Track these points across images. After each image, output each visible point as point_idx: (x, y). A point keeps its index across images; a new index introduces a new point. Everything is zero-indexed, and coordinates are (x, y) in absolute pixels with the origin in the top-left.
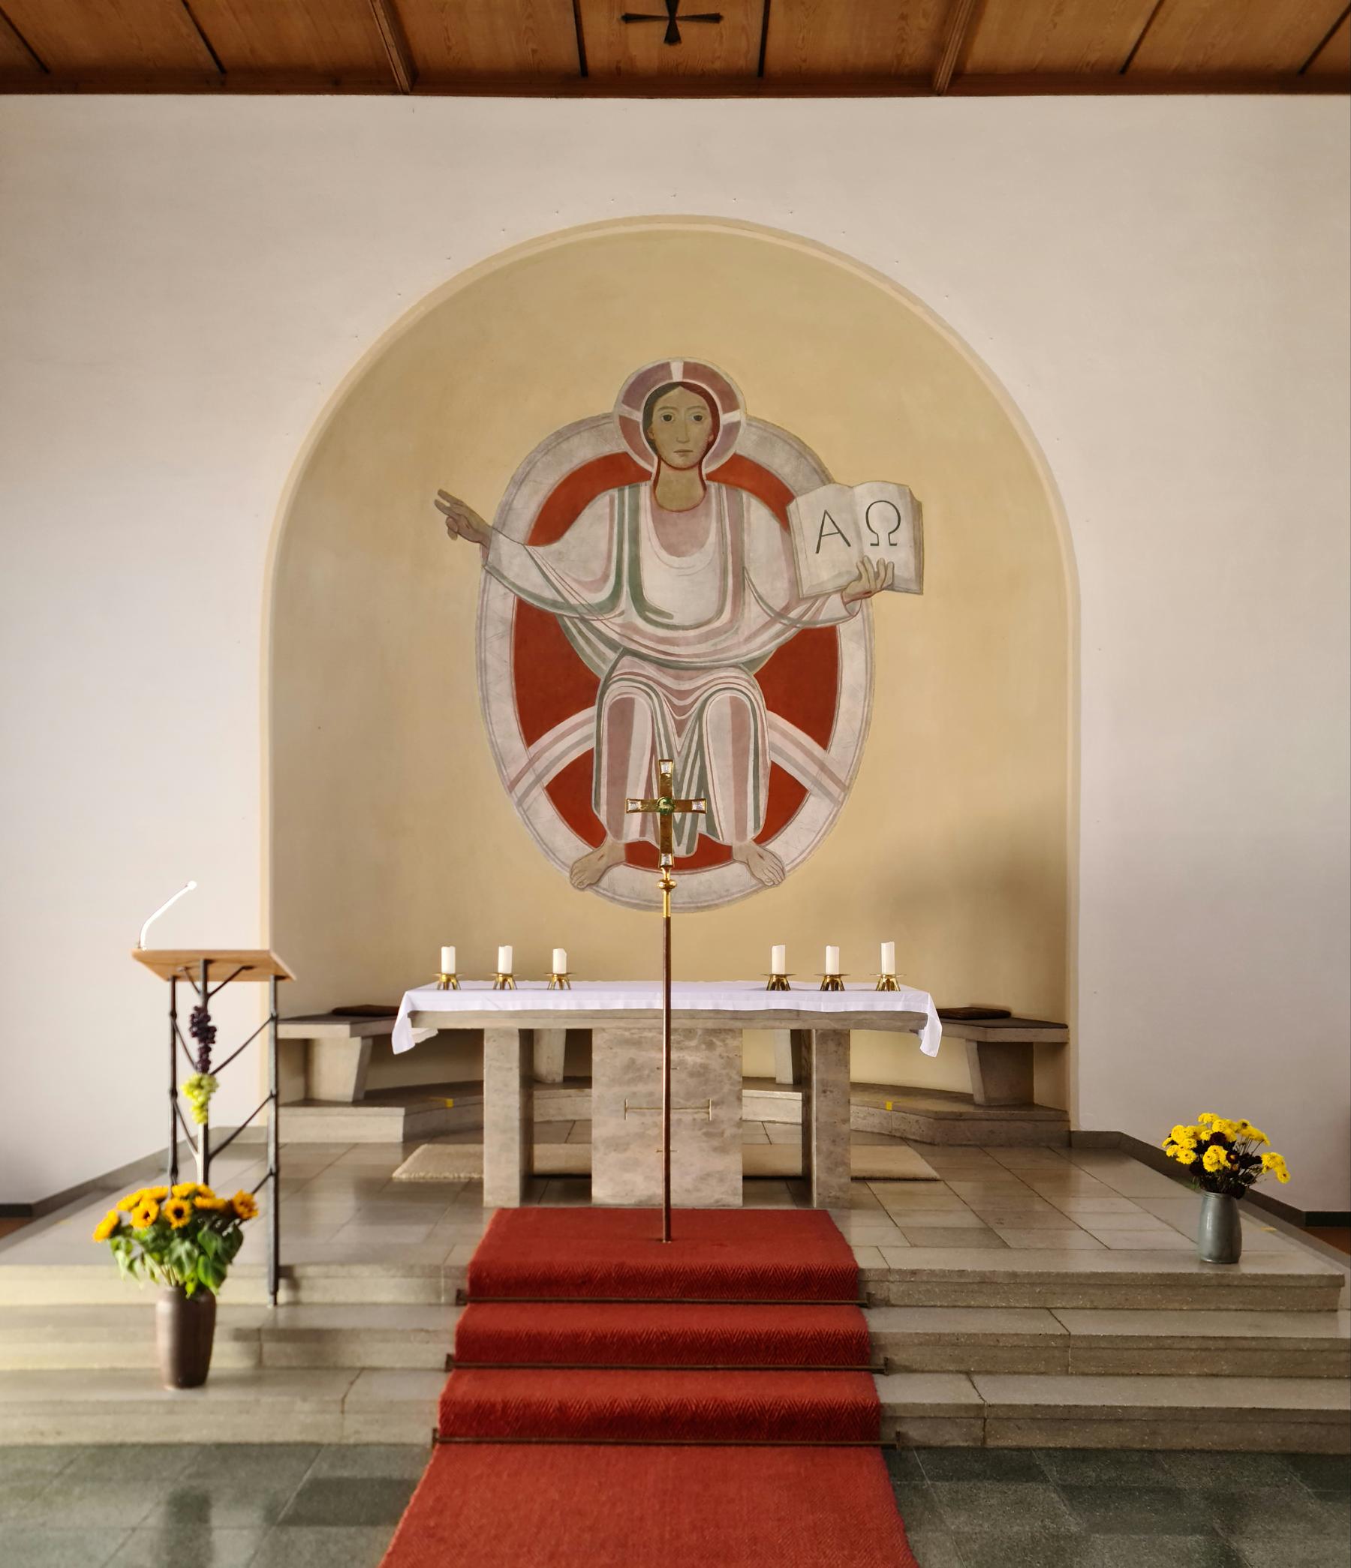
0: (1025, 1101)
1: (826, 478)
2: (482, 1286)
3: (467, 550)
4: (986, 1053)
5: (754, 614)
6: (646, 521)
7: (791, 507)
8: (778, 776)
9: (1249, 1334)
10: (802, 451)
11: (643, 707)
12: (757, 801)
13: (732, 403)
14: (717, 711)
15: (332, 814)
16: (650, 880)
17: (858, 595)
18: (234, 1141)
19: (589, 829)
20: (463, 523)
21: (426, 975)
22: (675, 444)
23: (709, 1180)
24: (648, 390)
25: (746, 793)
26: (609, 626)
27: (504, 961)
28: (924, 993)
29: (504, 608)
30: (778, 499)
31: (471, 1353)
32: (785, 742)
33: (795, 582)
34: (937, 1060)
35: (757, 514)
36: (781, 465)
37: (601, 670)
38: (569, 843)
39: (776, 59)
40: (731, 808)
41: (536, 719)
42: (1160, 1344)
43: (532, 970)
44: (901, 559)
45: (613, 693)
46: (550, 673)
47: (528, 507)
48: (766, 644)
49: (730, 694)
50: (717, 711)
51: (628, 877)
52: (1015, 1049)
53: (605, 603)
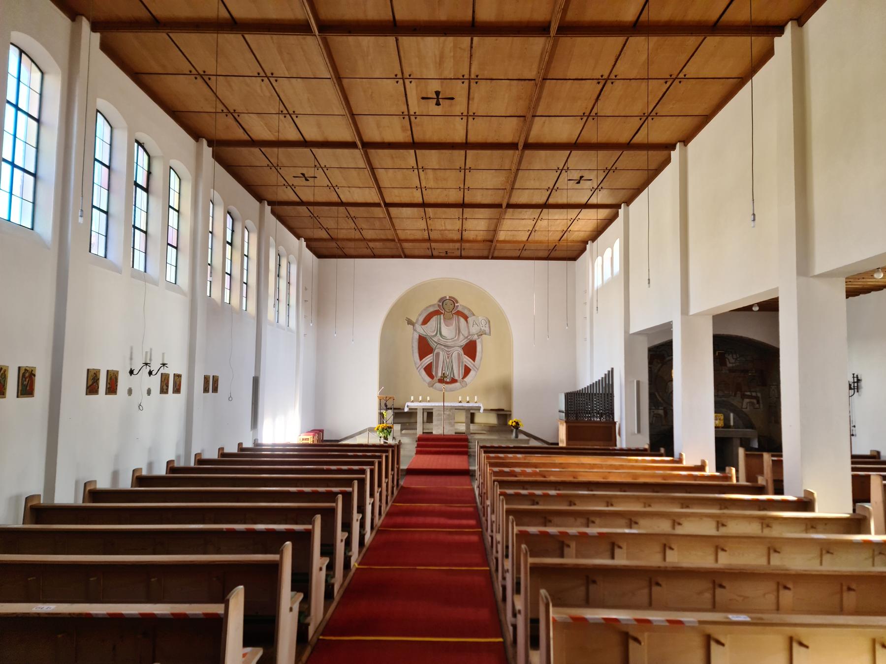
4: (499, 416)
5: (461, 337)
6: (442, 321)
9: (511, 445)
10: (470, 310)
12: (462, 371)
13: (457, 302)
14: (455, 355)
15: (389, 375)
16: (442, 386)
17: (481, 334)
20: (410, 322)
21: (409, 400)
22: (447, 308)
23: (449, 431)
24: (443, 300)
25: (266, 553)
26: (435, 339)
27: (420, 398)
29: (416, 336)
30: (466, 318)
31: (418, 446)
32: (467, 360)
34: (493, 420)
35: (462, 320)
36: (466, 312)
38: (428, 379)
40: (458, 373)
41: (422, 357)
43: (424, 400)
44: (487, 329)
46: (424, 347)
47: (421, 319)
48: (464, 343)
49: (457, 351)
50: (455, 355)
51: (438, 385)
52: (503, 415)
53: (434, 340)
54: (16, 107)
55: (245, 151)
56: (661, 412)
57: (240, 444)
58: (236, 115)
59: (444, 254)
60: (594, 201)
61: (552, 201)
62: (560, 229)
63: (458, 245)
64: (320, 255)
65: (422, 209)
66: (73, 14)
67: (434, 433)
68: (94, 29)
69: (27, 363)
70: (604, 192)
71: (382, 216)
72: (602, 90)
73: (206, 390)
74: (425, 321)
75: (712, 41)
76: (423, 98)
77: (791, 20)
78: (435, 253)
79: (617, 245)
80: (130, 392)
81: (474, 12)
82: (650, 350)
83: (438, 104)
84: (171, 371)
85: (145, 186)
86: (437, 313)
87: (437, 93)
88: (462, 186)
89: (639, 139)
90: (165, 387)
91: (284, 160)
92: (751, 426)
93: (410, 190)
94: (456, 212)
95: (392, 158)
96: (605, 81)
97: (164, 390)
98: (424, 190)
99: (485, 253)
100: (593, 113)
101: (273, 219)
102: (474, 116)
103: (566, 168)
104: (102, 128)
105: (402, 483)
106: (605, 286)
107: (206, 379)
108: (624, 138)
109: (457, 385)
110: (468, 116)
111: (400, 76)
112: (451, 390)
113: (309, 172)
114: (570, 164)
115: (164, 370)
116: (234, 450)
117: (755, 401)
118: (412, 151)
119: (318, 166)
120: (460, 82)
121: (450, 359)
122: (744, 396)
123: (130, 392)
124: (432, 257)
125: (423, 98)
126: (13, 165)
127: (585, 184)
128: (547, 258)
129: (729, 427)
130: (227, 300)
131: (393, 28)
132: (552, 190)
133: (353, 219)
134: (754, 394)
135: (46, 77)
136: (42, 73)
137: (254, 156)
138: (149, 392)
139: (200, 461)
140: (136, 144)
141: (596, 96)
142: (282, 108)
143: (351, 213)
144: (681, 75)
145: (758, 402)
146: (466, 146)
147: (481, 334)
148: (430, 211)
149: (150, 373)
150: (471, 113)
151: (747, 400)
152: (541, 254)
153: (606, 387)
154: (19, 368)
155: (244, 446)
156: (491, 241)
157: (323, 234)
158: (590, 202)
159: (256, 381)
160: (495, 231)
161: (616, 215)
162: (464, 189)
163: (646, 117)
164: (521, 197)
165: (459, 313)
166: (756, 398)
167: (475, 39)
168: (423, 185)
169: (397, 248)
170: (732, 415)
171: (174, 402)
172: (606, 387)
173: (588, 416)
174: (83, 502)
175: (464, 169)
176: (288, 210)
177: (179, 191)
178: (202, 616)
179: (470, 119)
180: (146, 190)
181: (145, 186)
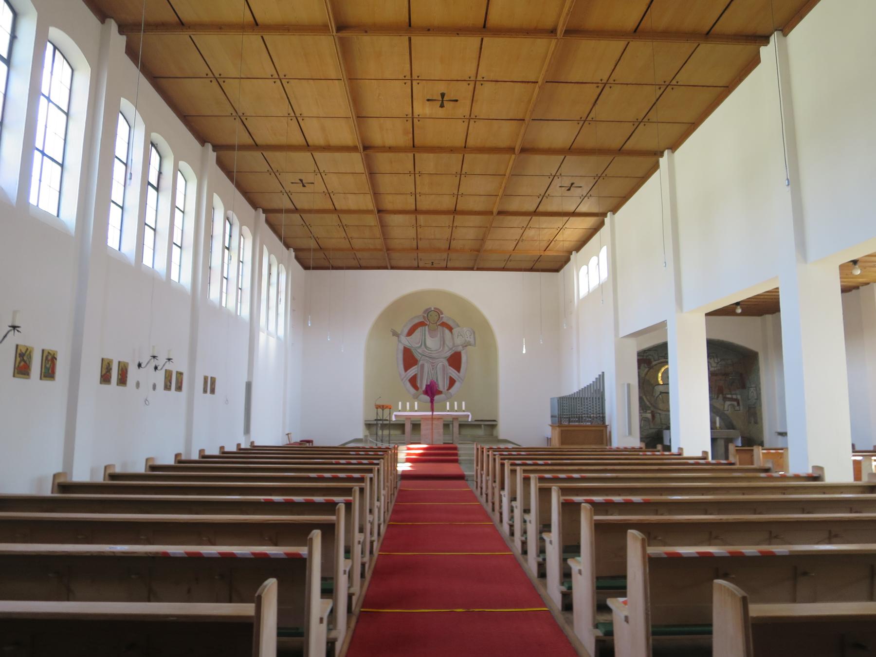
0: (492, 435)
3: (395, 338)
5: (446, 349)
6: (427, 333)
7: (436, 398)
10: (454, 321)
11: (426, 366)
14: (440, 366)
17: (466, 345)
18: (779, 172)
19: (416, 388)
20: (395, 334)
22: (432, 318)
24: (428, 311)
28: (714, 585)
29: (401, 348)
32: (452, 372)
35: (447, 331)
36: (450, 323)
40: (442, 385)
41: (406, 369)
42: (529, 493)
44: (472, 340)
45: (420, 363)
46: (409, 359)
47: (406, 331)
48: (449, 354)
50: (440, 366)
54: (48, 99)
55: (247, 154)
56: (649, 415)
57: (222, 448)
58: (243, 118)
59: (429, 265)
60: (583, 208)
61: (541, 209)
63: (445, 255)
65: (413, 217)
66: (103, 15)
68: (121, 31)
69: (49, 347)
70: (592, 199)
71: (373, 224)
73: (205, 391)
74: (410, 333)
75: (705, 48)
76: (428, 100)
77: (776, 30)
79: (604, 252)
80: (138, 385)
81: (486, 13)
82: (640, 354)
83: (442, 106)
84: (174, 367)
85: (156, 185)
87: (443, 95)
89: (629, 145)
94: (446, 220)
96: (604, 85)
97: (167, 387)
99: (471, 265)
100: (589, 118)
101: (266, 227)
102: (476, 119)
104: (122, 127)
108: (615, 142)
110: (470, 118)
111: (408, 77)
113: (308, 178)
114: (563, 170)
115: (169, 366)
116: (234, 449)
119: (318, 171)
120: (465, 83)
122: (725, 399)
123: (138, 385)
124: (418, 268)
125: (428, 100)
126: (43, 154)
128: (531, 270)
129: (716, 428)
130: (224, 305)
131: (408, 27)
132: (543, 196)
133: (344, 227)
134: (734, 397)
135: (76, 73)
136: (73, 70)
137: (254, 160)
141: (594, 100)
143: (343, 221)
144: (674, 82)
147: (466, 345)
148: (422, 218)
149: (156, 368)
151: (728, 403)
152: (523, 266)
153: (595, 394)
154: (43, 351)
156: (478, 251)
157: (312, 244)
158: (578, 210)
159: (249, 386)
160: (483, 240)
161: (602, 224)
162: (417, 226)
163: (637, 123)
164: (514, 205)
165: (444, 325)
166: (737, 400)
167: (485, 39)
169: (386, 258)
172: (595, 394)
176: (283, 218)
177: (187, 190)
178: (285, 556)
179: (472, 122)
180: (157, 189)
181: (156, 185)
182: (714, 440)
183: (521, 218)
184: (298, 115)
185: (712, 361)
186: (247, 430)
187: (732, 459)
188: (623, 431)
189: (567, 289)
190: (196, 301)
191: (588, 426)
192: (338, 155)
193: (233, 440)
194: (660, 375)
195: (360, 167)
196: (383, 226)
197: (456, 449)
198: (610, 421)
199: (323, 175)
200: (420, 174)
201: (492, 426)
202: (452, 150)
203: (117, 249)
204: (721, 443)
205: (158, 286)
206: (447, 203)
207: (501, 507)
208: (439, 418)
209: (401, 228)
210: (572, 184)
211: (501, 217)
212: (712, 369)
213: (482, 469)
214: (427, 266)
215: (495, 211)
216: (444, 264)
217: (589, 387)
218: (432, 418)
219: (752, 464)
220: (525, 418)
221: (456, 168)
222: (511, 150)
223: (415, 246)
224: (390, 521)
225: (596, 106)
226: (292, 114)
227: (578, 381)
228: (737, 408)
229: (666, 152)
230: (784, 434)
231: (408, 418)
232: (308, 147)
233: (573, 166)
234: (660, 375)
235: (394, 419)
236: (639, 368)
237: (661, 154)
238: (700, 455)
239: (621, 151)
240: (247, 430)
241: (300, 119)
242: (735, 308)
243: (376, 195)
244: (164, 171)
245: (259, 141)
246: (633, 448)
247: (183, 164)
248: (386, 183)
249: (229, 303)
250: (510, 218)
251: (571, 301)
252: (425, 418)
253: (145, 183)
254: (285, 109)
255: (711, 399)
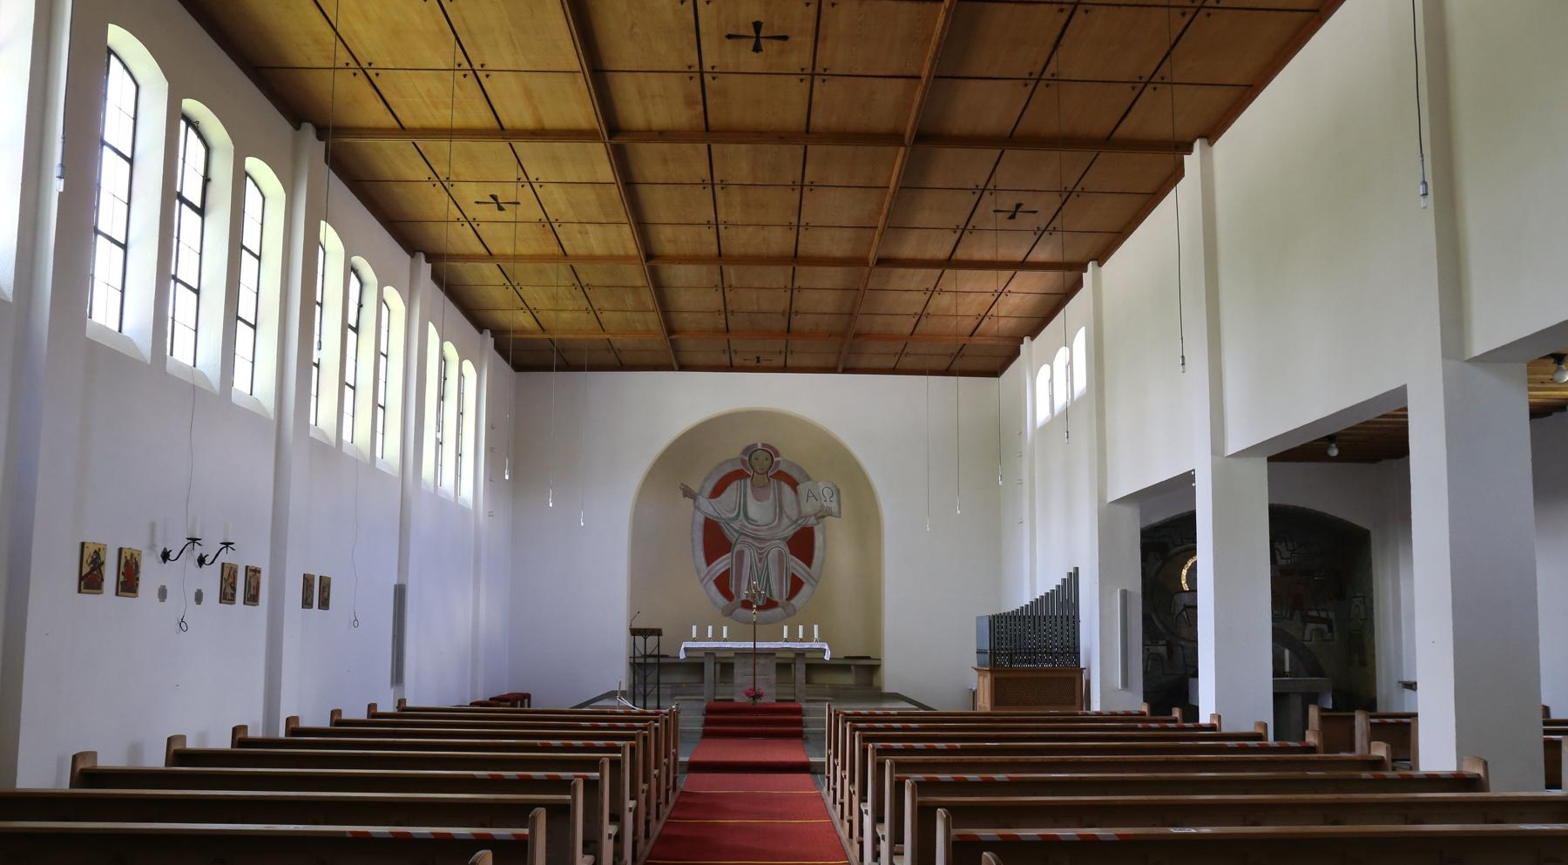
0: (871, 684)
1: (809, 479)
2: (709, 711)
3: (689, 501)
5: (786, 521)
6: (749, 490)
8: (794, 577)
10: (800, 469)
11: (747, 553)
13: (777, 454)
17: (822, 515)
19: (727, 594)
20: (687, 493)
22: (761, 463)
24: (750, 451)
29: (700, 519)
31: (707, 722)
32: (796, 566)
33: (800, 512)
35: (787, 489)
36: (795, 474)
37: (733, 540)
39: (818, 121)
40: (778, 590)
44: (834, 506)
45: (737, 548)
46: (715, 541)
47: (709, 487)
48: (790, 532)
49: (777, 548)
51: (741, 612)
55: (386, 144)
56: (1162, 650)
57: (372, 707)
59: (753, 363)
60: (1041, 254)
61: (961, 254)
62: (974, 310)
64: (519, 367)
67: (737, 699)
72: (1066, 26)
73: (307, 603)
74: (717, 492)
76: (729, 37)
78: (737, 361)
79: (1080, 340)
80: (163, 594)
83: (757, 49)
84: (241, 559)
85: (198, 204)
86: (738, 475)
88: (794, 220)
89: (1126, 129)
90: (229, 590)
91: (461, 168)
92: (1319, 672)
93: (696, 228)
95: (665, 161)
97: (227, 596)
98: (721, 227)
99: (831, 362)
100: (1047, 75)
102: (827, 75)
103: (990, 186)
104: (118, 85)
105: (681, 785)
106: (1047, 427)
107: (308, 581)
108: (1099, 125)
109: (778, 611)
110: (812, 74)
112: (767, 622)
115: (226, 557)
117: (1325, 627)
118: (703, 147)
119: (525, 180)
121: (761, 564)
122: (1306, 619)
123: (163, 594)
124: (730, 368)
125: (729, 37)
127: (1024, 221)
128: (947, 372)
129: (1284, 674)
130: (346, 437)
134: (1323, 615)
138: (199, 597)
139: (294, 728)
140: (183, 124)
141: (1053, 41)
142: (461, 58)
145: (1331, 629)
146: (807, 135)
148: (732, 272)
149: (201, 561)
150: (818, 70)
151: (1311, 626)
152: (934, 363)
155: (380, 710)
158: (1031, 258)
159: (400, 593)
161: (1078, 284)
162: (723, 286)
163: (1141, 85)
164: (909, 247)
166: (1327, 621)
168: (721, 217)
169: (674, 354)
170: (1287, 652)
171: (249, 620)
173: (1030, 647)
174: (72, 785)
175: (801, 186)
179: (817, 80)
180: (201, 211)
181: (198, 204)
182: (1279, 698)
183: (923, 271)
184: (477, 66)
185: (1282, 547)
186: (398, 677)
187: (1311, 738)
188: (1108, 676)
189: (1018, 408)
190: (284, 428)
191: (1047, 670)
192: (560, 147)
193: (364, 692)
194: (1184, 572)
195: (605, 171)
196: (659, 287)
197: (799, 711)
198: (1089, 661)
199: (536, 186)
200: (725, 185)
201: (867, 668)
202: (781, 137)
203: (116, 329)
204: (1296, 702)
205: (206, 401)
206: (778, 240)
207: (861, 833)
208: (770, 653)
209: (693, 290)
210: (1018, 206)
211: (884, 270)
212: (1281, 562)
213: (836, 756)
214: (748, 363)
215: (872, 257)
216: (779, 361)
217: (1049, 596)
218: (756, 653)
219: (1352, 749)
220: (932, 654)
221: (792, 174)
222: (893, 138)
223: (722, 325)
224: (649, 857)
225: (1061, 51)
226: (466, 65)
227: (1030, 584)
228: (1329, 636)
229: (1197, 145)
230: (1412, 686)
231: (710, 653)
232: (501, 132)
233: (1016, 168)
234: (1184, 572)
235: (682, 656)
236: (1144, 560)
237: (1189, 149)
238: (1249, 728)
239: (1109, 142)
240: (398, 677)
241: (481, 75)
242: (1328, 447)
243: (641, 226)
244: (213, 174)
245: (409, 122)
246: (1127, 714)
247: (253, 164)
248: (658, 202)
249: (358, 433)
250: (901, 271)
251: (1021, 433)
252: (741, 653)
253: (171, 196)
254: (445, 55)
255: (1275, 618)
